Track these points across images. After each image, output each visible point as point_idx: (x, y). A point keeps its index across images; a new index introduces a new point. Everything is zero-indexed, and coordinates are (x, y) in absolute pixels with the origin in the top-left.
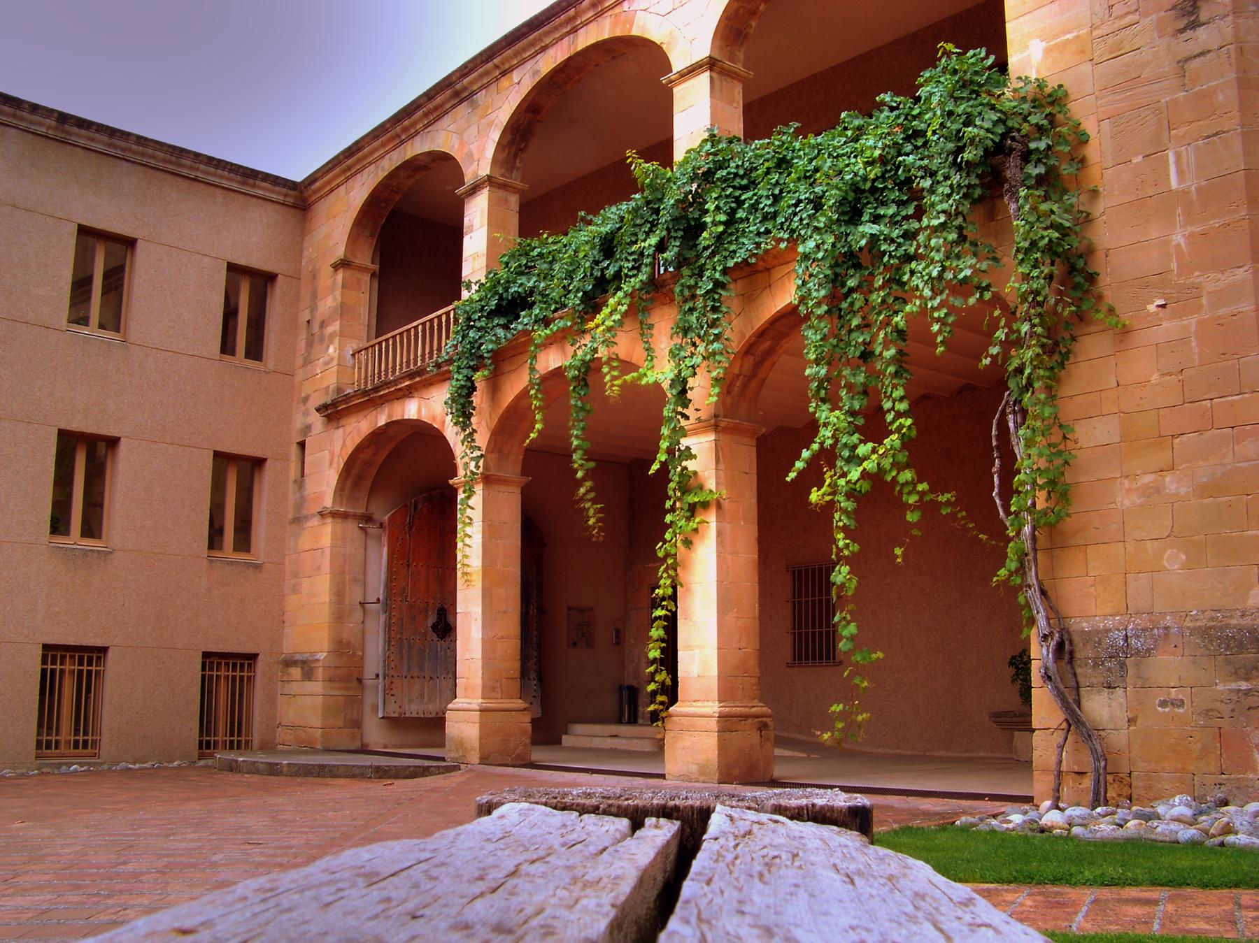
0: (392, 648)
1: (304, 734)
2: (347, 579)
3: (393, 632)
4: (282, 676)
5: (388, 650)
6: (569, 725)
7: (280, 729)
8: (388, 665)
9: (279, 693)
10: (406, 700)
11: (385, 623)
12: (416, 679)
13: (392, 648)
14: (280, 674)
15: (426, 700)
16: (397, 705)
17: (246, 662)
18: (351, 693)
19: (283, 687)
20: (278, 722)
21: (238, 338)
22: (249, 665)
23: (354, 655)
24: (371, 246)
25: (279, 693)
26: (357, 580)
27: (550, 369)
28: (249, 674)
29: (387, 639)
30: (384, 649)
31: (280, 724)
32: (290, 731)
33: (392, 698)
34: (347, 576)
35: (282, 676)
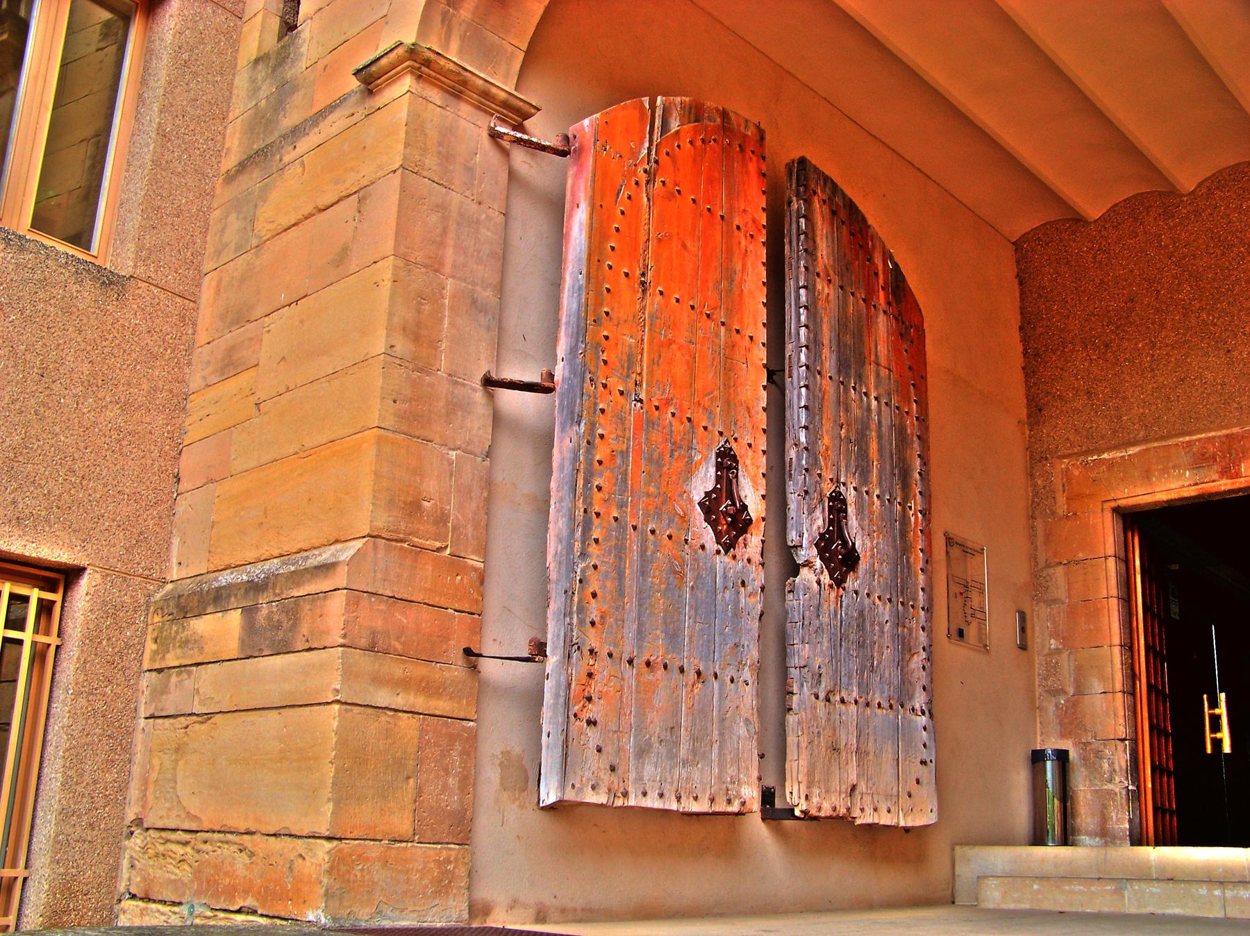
0: (593, 549)
1: (243, 859)
2: (448, 292)
3: (598, 496)
4: (163, 649)
5: (584, 555)
6: (959, 850)
7: (137, 840)
8: (581, 610)
9: (143, 712)
10: (630, 744)
11: (575, 458)
12: (660, 672)
13: (593, 549)
14: (151, 646)
15: (683, 751)
16: (604, 763)
17: (35, 594)
18: (442, 706)
19: (159, 692)
20: (130, 816)
21: (31, 721)
22: (45, 608)
23: (456, 563)
24: (244, 153)
25: (143, 712)
26: (475, 305)
27: (585, 223)
28: (42, 639)
29: (580, 514)
30: (570, 547)
31: (139, 822)
32: (180, 850)
33: (590, 731)
34: (450, 284)
35: (163, 649)
